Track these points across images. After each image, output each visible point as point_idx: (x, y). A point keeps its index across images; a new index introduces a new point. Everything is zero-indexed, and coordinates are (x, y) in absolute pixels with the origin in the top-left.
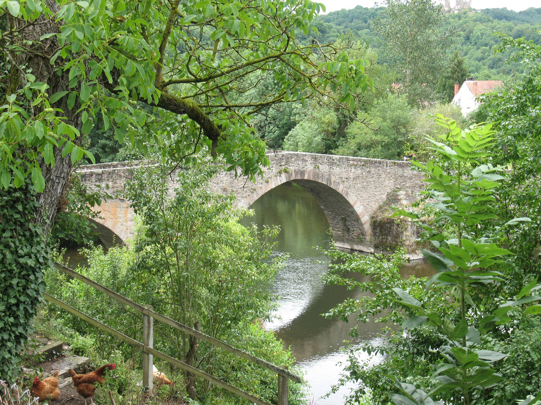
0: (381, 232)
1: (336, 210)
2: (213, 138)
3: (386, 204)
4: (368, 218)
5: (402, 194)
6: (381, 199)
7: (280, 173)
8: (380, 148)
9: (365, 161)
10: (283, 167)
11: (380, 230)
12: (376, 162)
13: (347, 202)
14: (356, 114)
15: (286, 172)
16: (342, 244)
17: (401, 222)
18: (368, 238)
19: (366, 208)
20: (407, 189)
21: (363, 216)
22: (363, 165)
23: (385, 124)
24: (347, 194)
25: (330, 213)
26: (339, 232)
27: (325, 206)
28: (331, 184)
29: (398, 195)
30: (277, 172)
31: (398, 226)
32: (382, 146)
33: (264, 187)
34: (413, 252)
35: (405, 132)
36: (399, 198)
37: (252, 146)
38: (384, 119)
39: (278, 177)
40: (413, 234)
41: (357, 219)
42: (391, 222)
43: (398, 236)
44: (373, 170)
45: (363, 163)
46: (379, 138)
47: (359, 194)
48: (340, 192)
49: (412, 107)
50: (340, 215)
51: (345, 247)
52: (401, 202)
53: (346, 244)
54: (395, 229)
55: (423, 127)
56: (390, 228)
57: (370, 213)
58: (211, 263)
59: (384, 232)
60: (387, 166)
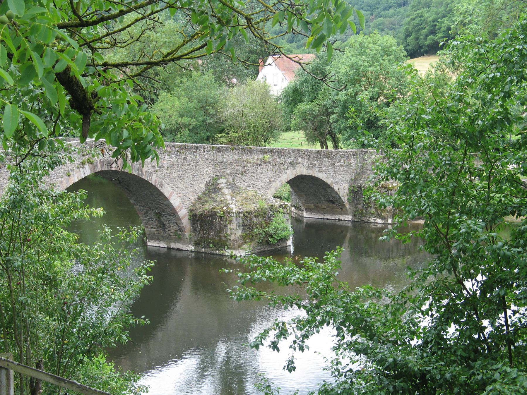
0: (201, 226)
1: (149, 204)
2: (86, 112)
3: (205, 194)
4: (186, 212)
5: (222, 182)
6: (199, 189)
7: (83, 164)
8: (187, 132)
9: (180, 147)
10: (87, 157)
11: (200, 225)
12: (192, 147)
13: (161, 194)
14: (157, 95)
15: (90, 162)
16: (157, 242)
17: (224, 213)
18: (187, 234)
19: (183, 200)
20: (228, 177)
21: (180, 210)
22: (178, 151)
23: (191, 104)
24: (161, 185)
25: (142, 208)
26: (152, 229)
27: (135, 200)
28: (142, 174)
29: (218, 184)
30: (79, 163)
31: (221, 219)
32: (189, 130)
33: (65, 182)
34: (240, 247)
35: (214, 113)
36: (220, 187)
37: (143, 121)
38: (190, 99)
39: (81, 169)
40: (239, 226)
41: (174, 213)
42: (212, 214)
43: (221, 230)
44: (189, 156)
45: (177, 149)
46: (185, 120)
47: (174, 185)
48: (153, 183)
49: (220, 85)
50: (153, 210)
51: (161, 245)
52: (223, 191)
53: (162, 242)
54: (217, 222)
55: (233, 106)
56: (212, 222)
57: (188, 205)
58: (52, 281)
59: (205, 227)
60: (204, 151)
